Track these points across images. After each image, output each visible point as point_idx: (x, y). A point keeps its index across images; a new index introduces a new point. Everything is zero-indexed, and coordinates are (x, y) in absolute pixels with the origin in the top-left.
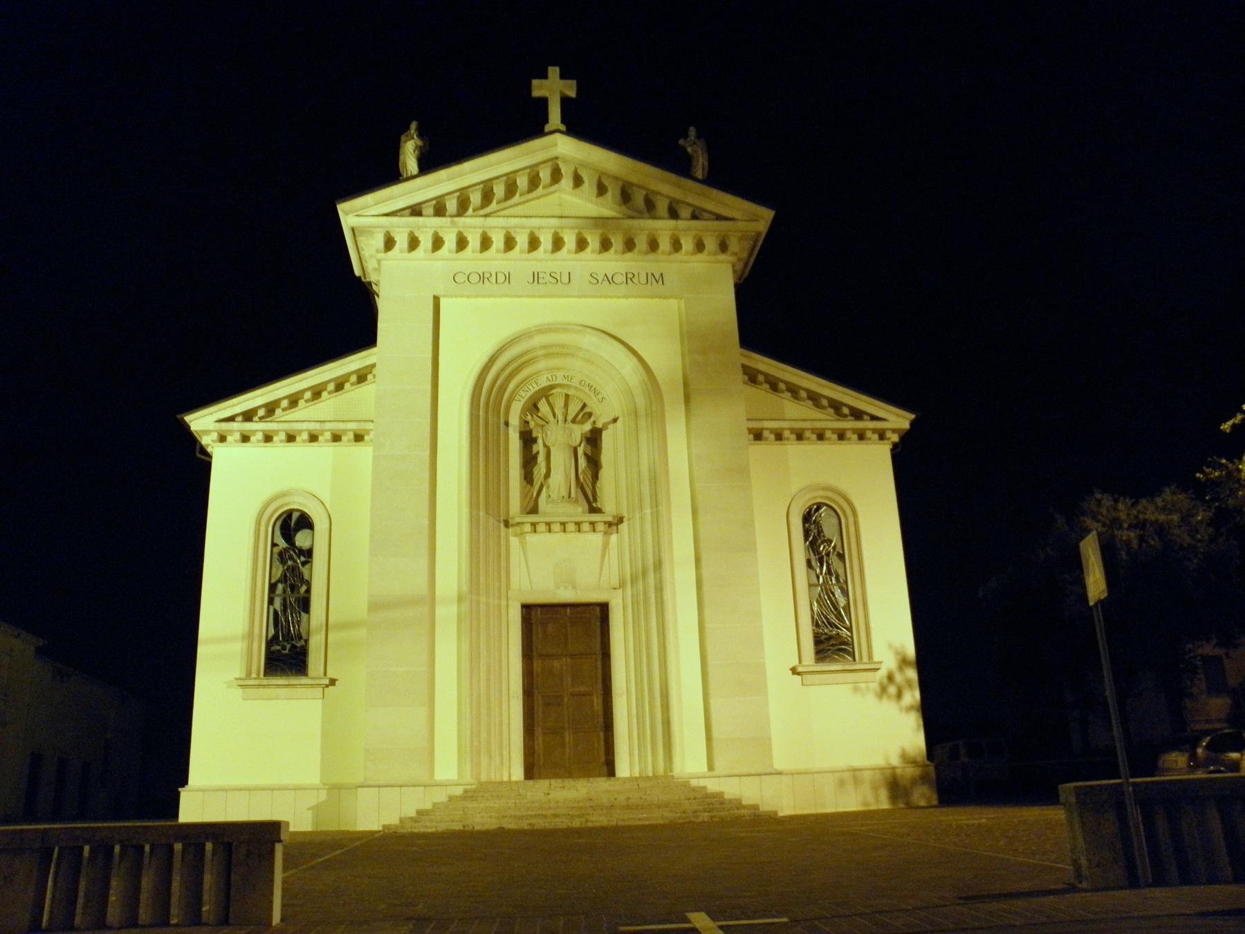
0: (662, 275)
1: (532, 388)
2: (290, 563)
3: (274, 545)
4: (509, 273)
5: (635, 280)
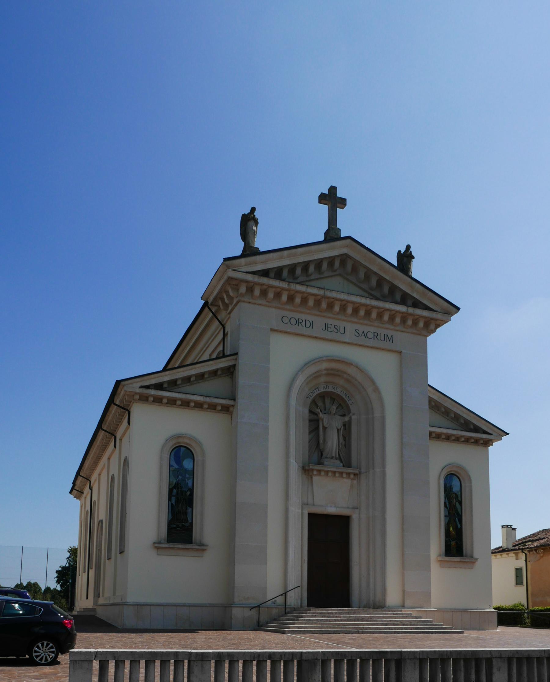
0: (392, 336)
1: (316, 392)
2: (180, 477)
3: (170, 466)
4: (312, 321)
5: (378, 337)
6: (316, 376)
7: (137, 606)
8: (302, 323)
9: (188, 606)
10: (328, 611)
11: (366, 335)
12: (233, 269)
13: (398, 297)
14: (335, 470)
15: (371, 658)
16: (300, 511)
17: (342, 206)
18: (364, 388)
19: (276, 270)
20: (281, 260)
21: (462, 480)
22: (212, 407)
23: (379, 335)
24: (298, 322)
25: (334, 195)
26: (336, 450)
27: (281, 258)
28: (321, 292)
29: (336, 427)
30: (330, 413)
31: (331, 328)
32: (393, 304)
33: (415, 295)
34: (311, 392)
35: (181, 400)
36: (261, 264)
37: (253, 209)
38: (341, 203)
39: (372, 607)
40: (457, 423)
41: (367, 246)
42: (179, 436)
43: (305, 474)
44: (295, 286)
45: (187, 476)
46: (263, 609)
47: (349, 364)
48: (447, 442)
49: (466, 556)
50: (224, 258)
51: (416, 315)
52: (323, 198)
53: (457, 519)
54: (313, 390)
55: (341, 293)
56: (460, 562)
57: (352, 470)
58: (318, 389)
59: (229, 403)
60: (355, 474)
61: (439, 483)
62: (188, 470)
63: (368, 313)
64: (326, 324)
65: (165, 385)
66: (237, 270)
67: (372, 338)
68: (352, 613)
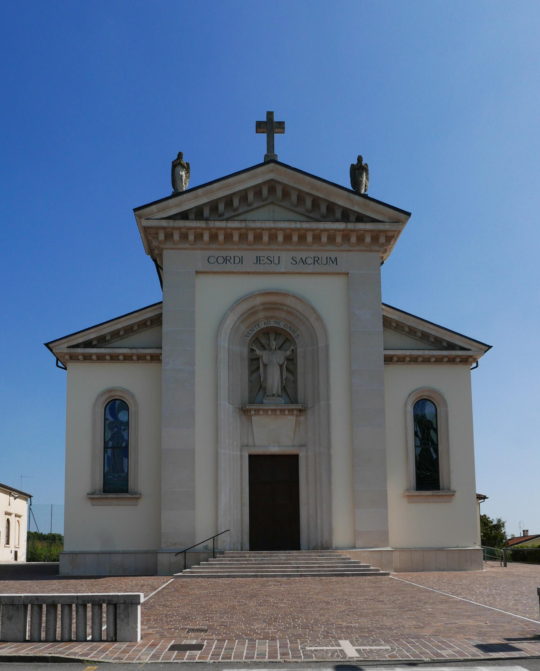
0: (336, 258)
2: (115, 430)
3: (105, 419)
4: (242, 257)
6: (252, 312)
7: (72, 555)
8: (230, 260)
9: (121, 553)
10: (245, 554)
11: (304, 261)
12: (146, 218)
13: (338, 214)
14: (274, 407)
15: (73, 603)
16: (239, 453)
17: (280, 130)
18: (306, 318)
19: (195, 210)
20: (197, 199)
21: (436, 404)
22: (141, 358)
23: (320, 259)
24: (225, 260)
25: (271, 121)
26: (278, 387)
27: (197, 197)
28: (243, 225)
29: (278, 363)
30: (271, 349)
31: (263, 260)
32: (335, 223)
33: (356, 209)
34: (250, 330)
35: (110, 354)
36: (176, 207)
37: (360, 159)
38: (278, 128)
39: (320, 548)
40: (427, 342)
41: (293, 167)
42: (110, 391)
43: (244, 415)
44: (214, 224)
45: (123, 427)
46: (190, 554)
47: (285, 295)
48: (415, 364)
49: (443, 489)
50: (134, 208)
51: (360, 230)
52: (260, 126)
53: (431, 448)
54: (252, 328)
55: (266, 221)
56: (433, 495)
57: (294, 405)
58: (258, 326)
59: (157, 352)
60: (300, 411)
61: (405, 411)
62: (123, 421)
63: (302, 238)
64: (257, 257)
65: (94, 343)
66: (150, 218)
67: (312, 263)
68: (268, 555)
